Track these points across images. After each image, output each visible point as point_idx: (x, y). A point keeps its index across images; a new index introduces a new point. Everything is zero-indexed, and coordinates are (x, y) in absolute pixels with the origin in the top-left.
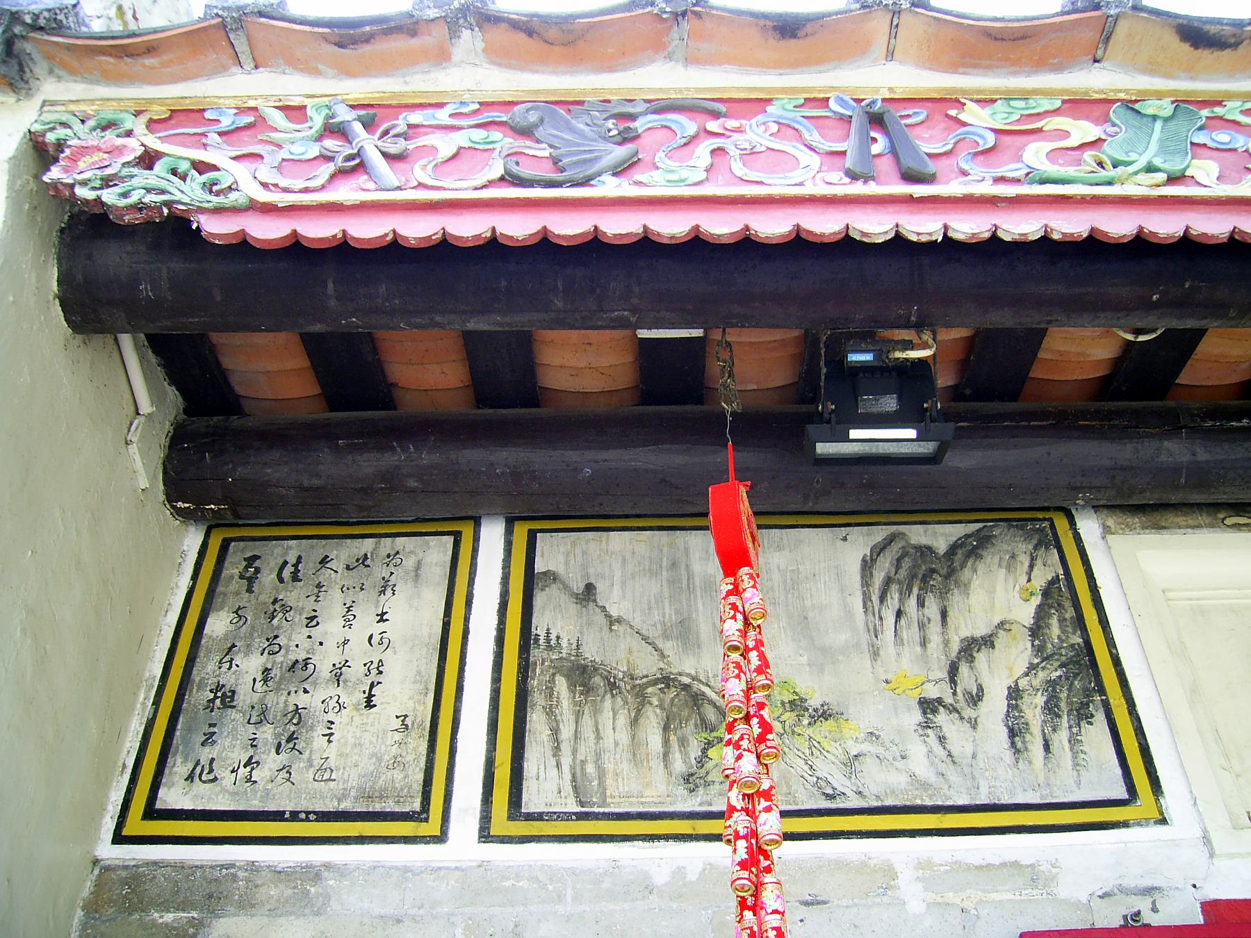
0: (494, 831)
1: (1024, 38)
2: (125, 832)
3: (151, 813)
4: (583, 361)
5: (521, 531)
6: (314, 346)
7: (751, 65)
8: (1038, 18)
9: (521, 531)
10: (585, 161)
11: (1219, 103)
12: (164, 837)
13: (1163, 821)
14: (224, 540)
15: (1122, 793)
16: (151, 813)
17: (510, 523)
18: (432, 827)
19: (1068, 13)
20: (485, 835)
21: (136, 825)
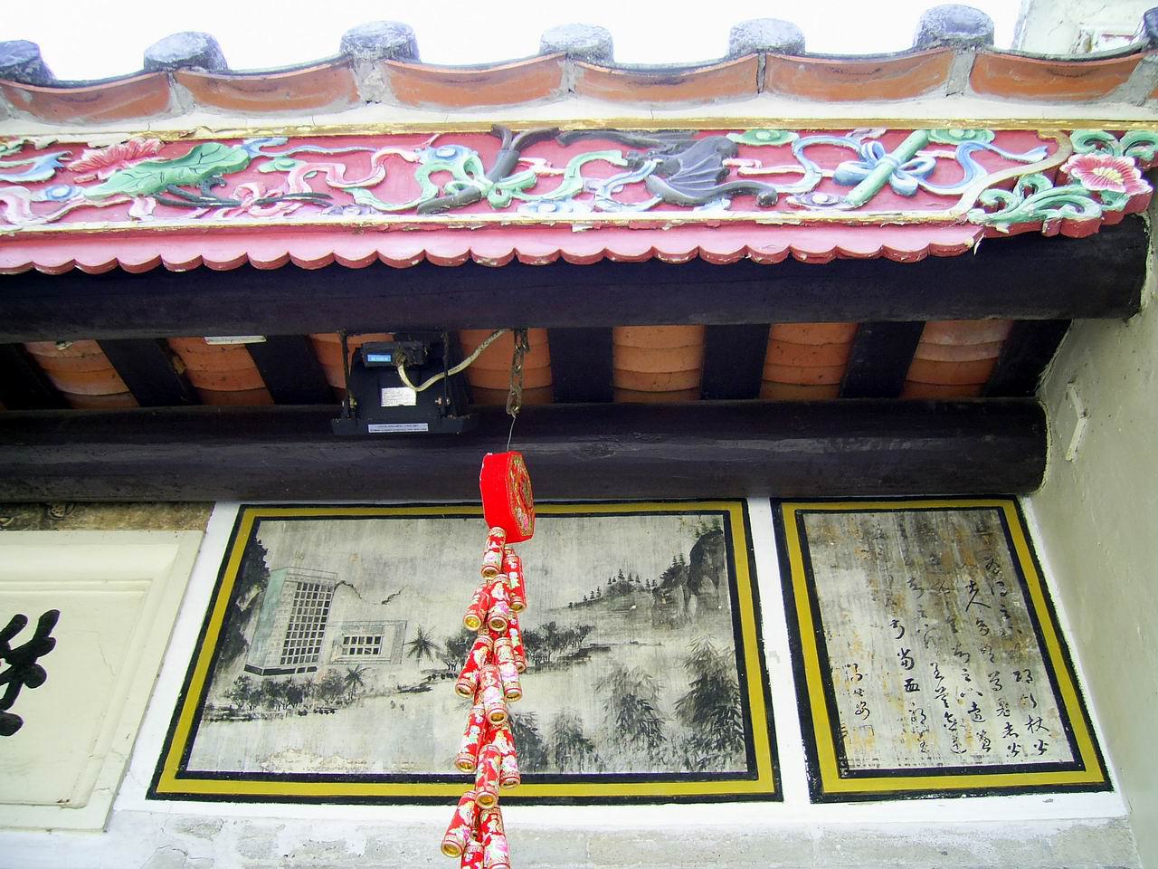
0: (769, 788)
1: (481, 80)
2: (160, 790)
3: (1078, 765)
4: (657, 356)
5: (250, 515)
6: (559, 343)
7: (499, 103)
8: (508, 63)
9: (250, 515)
10: (690, 186)
11: (841, 132)
12: (198, 795)
13: (152, 795)
14: (256, 518)
15: (193, 766)
16: (1078, 765)
17: (776, 504)
18: (832, 783)
19: (546, 54)
20: (818, 795)
21: (168, 784)
